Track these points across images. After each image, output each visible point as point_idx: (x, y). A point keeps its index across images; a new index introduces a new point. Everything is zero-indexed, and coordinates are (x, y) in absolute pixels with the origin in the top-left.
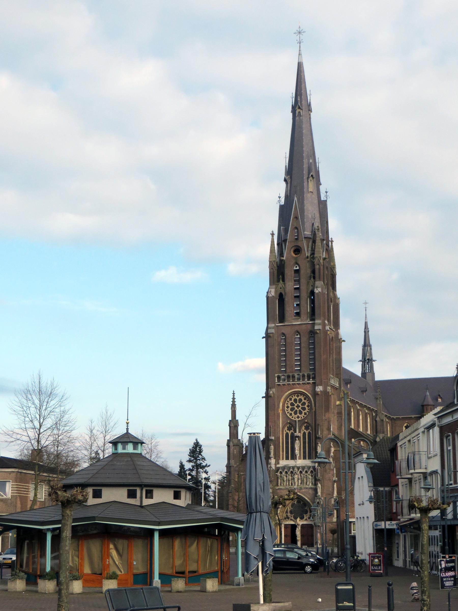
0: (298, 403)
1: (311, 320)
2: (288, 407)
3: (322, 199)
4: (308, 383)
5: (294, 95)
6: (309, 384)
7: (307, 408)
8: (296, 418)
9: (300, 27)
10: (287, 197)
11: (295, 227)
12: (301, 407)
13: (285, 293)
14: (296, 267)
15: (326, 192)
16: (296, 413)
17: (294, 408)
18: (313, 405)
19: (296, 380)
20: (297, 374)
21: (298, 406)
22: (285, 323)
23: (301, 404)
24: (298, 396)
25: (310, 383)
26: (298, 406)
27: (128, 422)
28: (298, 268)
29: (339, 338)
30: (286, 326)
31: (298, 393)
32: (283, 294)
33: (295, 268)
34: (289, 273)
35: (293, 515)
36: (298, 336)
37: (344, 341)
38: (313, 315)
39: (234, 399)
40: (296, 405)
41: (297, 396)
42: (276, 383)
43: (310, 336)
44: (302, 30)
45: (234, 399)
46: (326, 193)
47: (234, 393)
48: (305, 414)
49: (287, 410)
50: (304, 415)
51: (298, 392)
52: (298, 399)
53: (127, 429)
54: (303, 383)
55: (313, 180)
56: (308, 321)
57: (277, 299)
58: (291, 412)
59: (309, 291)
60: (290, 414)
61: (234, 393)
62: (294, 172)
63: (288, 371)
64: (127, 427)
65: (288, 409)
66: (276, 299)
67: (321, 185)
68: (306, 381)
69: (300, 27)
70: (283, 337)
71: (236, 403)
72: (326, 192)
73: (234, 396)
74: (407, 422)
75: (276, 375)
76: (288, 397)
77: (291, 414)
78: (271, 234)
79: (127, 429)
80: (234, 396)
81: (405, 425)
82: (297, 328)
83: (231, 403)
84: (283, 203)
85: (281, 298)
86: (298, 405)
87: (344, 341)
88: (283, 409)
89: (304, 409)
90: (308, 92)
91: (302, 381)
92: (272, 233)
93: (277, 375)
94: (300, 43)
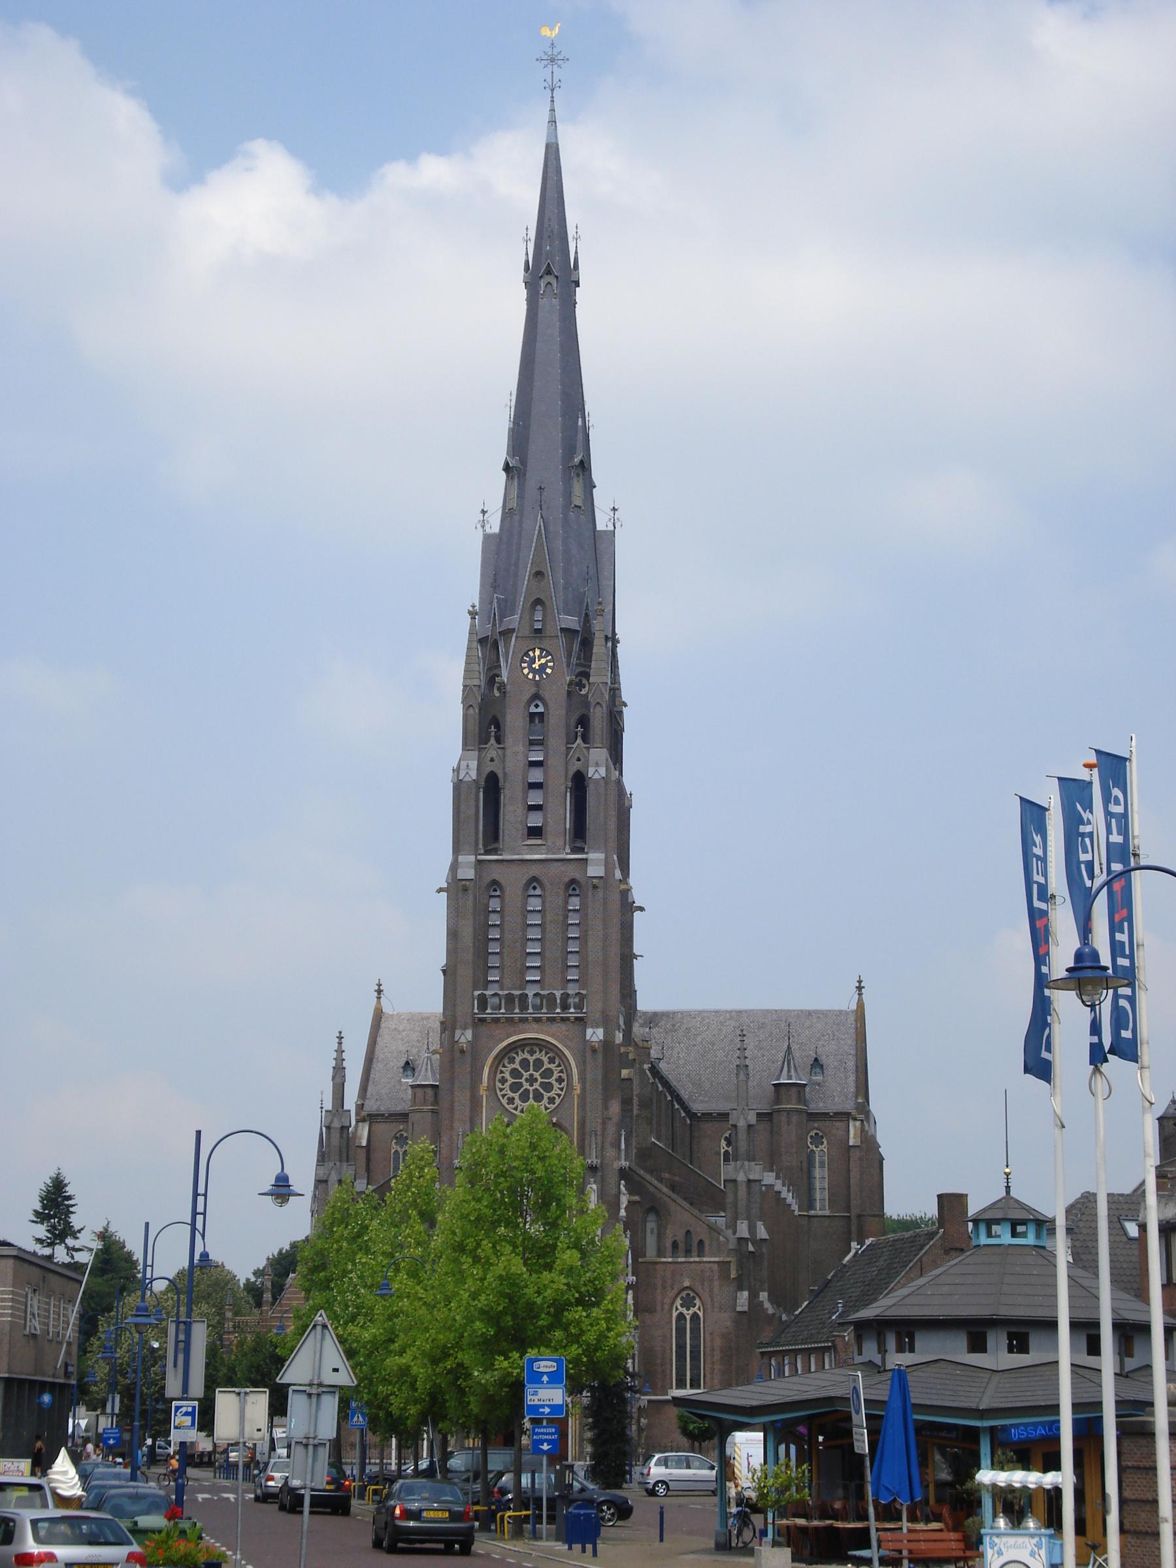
0: (531, 1071)
1: (575, 850)
2: (551, 1100)
3: (600, 526)
4: (563, 1020)
5: (532, 234)
6: (568, 1022)
7: (518, 1060)
8: (548, 1106)
9: (553, 44)
10: (508, 514)
11: (535, 598)
12: (538, 1083)
13: (505, 774)
14: (537, 706)
15: (483, 510)
16: (538, 1097)
17: (521, 1085)
18: (576, 1077)
19: (531, 1010)
20: (535, 992)
21: (531, 1080)
22: (501, 855)
23: (540, 1075)
24: (532, 1053)
25: (568, 1019)
26: (531, 1080)
27: (1007, 1170)
28: (541, 709)
29: (630, 900)
30: (505, 863)
31: (533, 1044)
32: (500, 775)
33: (533, 709)
34: (515, 720)
35: (493, 726)
36: (538, 892)
37: (641, 909)
38: (579, 833)
39: (340, 1051)
40: (526, 1075)
41: (528, 1052)
42: (476, 1014)
43: (571, 892)
44: (559, 53)
45: (340, 1051)
46: (482, 515)
47: (342, 1035)
48: (551, 1100)
49: (516, 1109)
50: (549, 1104)
51: (532, 1042)
52: (531, 1059)
53: (1008, 1188)
54: (549, 1019)
55: (583, 475)
56: (567, 854)
57: (481, 790)
58: (511, 1094)
59: (571, 774)
60: (508, 1098)
61: (342, 1035)
62: (532, 448)
63: (507, 981)
64: (1008, 1183)
65: (503, 1085)
66: (479, 788)
67: (595, 487)
68: (558, 1013)
69: (553, 44)
70: (495, 890)
71: (345, 1064)
72: (483, 510)
73: (340, 1043)
74: (816, 1125)
75: (477, 993)
76: (505, 1055)
77: (511, 1101)
78: (470, 613)
79: (1008, 1188)
80: (340, 1043)
81: (813, 1133)
82: (534, 871)
83: (333, 1063)
84: (494, 526)
85: (492, 786)
86: (531, 1075)
87: (641, 909)
88: (492, 1089)
89: (548, 1087)
90: (571, 232)
91: (545, 1013)
92: (471, 609)
93: (479, 992)
94: (552, 90)
